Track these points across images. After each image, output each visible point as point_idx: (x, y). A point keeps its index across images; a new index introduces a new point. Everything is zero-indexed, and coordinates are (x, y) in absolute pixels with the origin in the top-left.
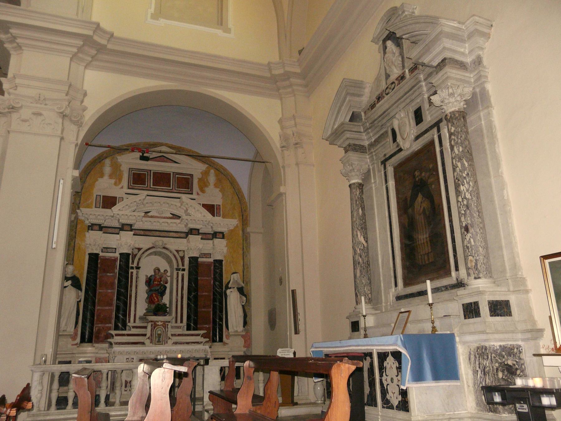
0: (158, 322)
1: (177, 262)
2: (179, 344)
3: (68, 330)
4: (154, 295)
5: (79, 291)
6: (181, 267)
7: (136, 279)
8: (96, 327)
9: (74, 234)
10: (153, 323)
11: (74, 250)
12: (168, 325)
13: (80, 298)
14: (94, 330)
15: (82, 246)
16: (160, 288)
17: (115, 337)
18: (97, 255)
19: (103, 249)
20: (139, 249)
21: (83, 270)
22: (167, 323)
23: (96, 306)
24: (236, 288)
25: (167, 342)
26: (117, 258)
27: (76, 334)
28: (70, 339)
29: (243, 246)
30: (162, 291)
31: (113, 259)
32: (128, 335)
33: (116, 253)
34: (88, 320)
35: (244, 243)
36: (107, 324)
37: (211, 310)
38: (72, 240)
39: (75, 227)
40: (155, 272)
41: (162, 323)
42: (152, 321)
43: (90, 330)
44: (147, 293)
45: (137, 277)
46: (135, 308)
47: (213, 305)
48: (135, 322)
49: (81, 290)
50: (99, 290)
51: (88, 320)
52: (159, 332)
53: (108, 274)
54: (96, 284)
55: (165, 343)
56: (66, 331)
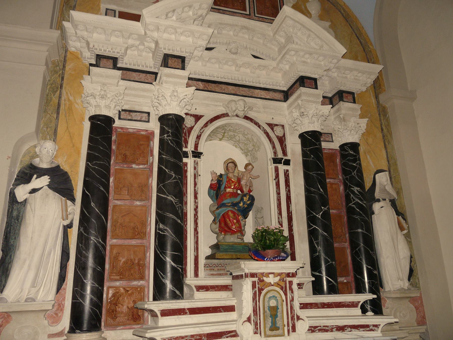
0: (268, 275)
1: (274, 147)
2: (320, 330)
3: (40, 296)
4: (231, 214)
5: (69, 203)
6: (280, 155)
7: (195, 179)
8: (108, 288)
9: (59, 80)
10: (256, 279)
11: (58, 113)
12: (291, 283)
13: (70, 217)
14: (105, 296)
15: (76, 106)
16: (242, 199)
17: (164, 321)
18: (109, 120)
19: (122, 113)
20: (198, 118)
21: (79, 153)
22: (289, 279)
23: (108, 238)
24: (387, 200)
25: (294, 330)
26: (153, 133)
27: (60, 307)
28: (46, 322)
29: (381, 125)
30: (246, 206)
31: (142, 135)
32: (194, 311)
33: (148, 121)
34: (90, 273)
35: (382, 118)
36: (135, 279)
37: (347, 245)
38: (55, 92)
39: (62, 67)
40: (227, 168)
41: (277, 279)
42: (253, 275)
43: (95, 299)
44: (213, 212)
45: (195, 175)
46: (197, 243)
47: (350, 234)
48: (196, 275)
49: (73, 200)
50: (113, 202)
51: (90, 273)
52: (273, 303)
53: (134, 166)
54: (107, 187)
55: (288, 331)
56: (33, 300)
